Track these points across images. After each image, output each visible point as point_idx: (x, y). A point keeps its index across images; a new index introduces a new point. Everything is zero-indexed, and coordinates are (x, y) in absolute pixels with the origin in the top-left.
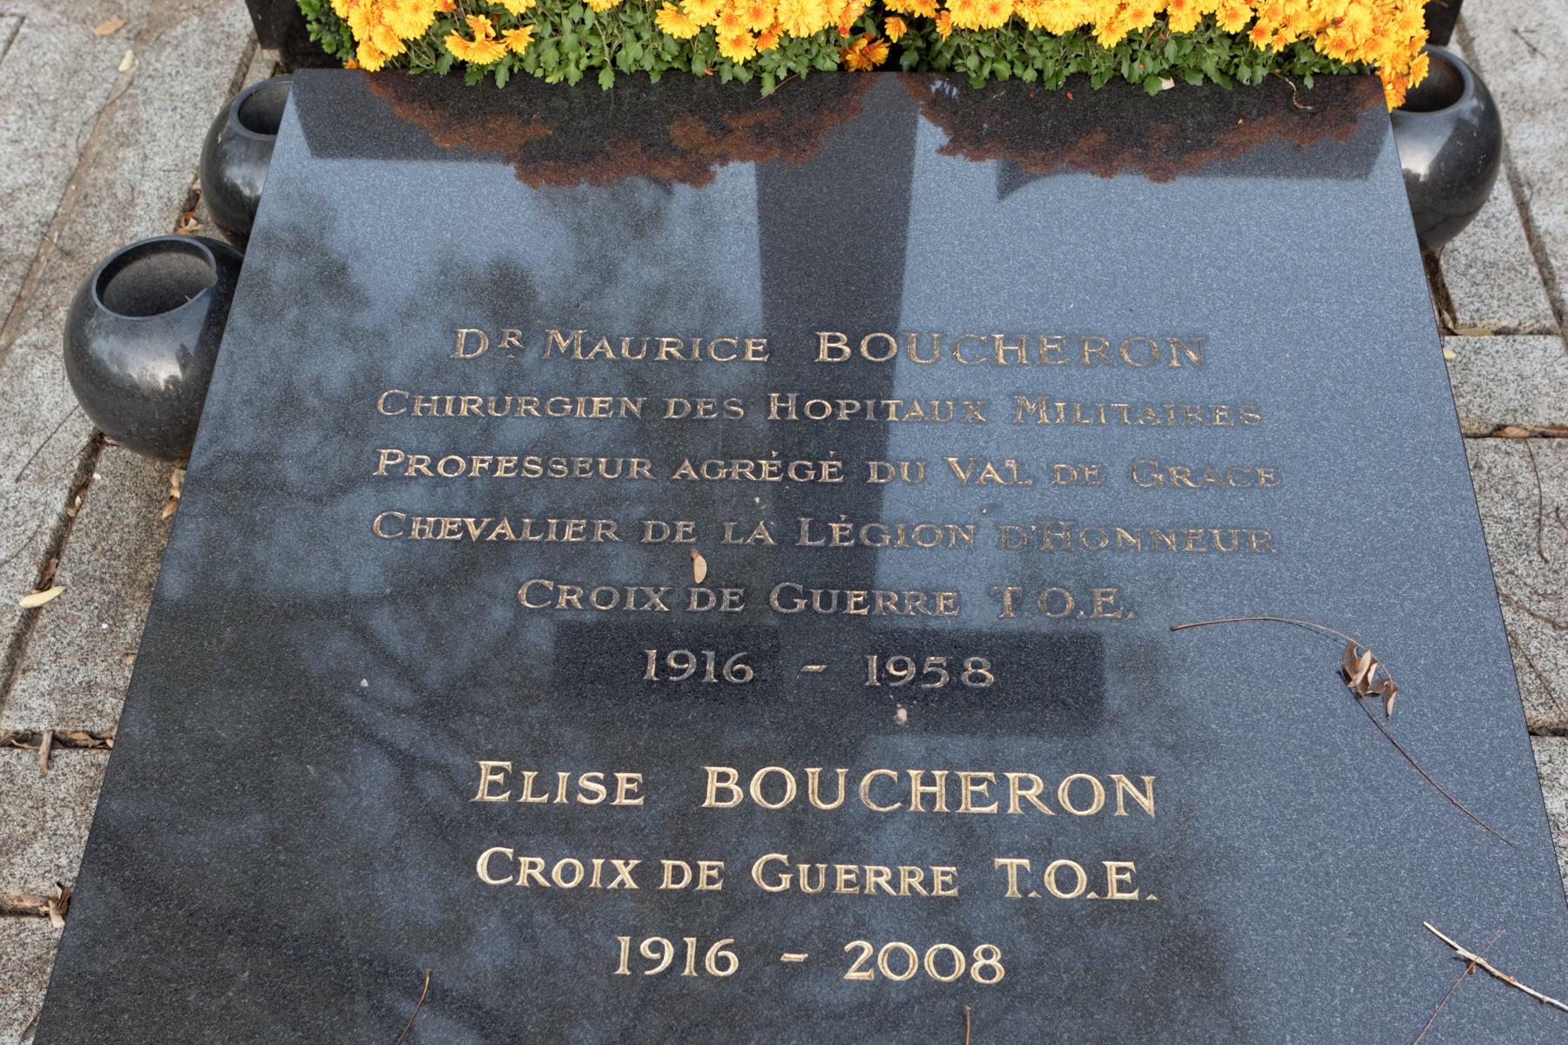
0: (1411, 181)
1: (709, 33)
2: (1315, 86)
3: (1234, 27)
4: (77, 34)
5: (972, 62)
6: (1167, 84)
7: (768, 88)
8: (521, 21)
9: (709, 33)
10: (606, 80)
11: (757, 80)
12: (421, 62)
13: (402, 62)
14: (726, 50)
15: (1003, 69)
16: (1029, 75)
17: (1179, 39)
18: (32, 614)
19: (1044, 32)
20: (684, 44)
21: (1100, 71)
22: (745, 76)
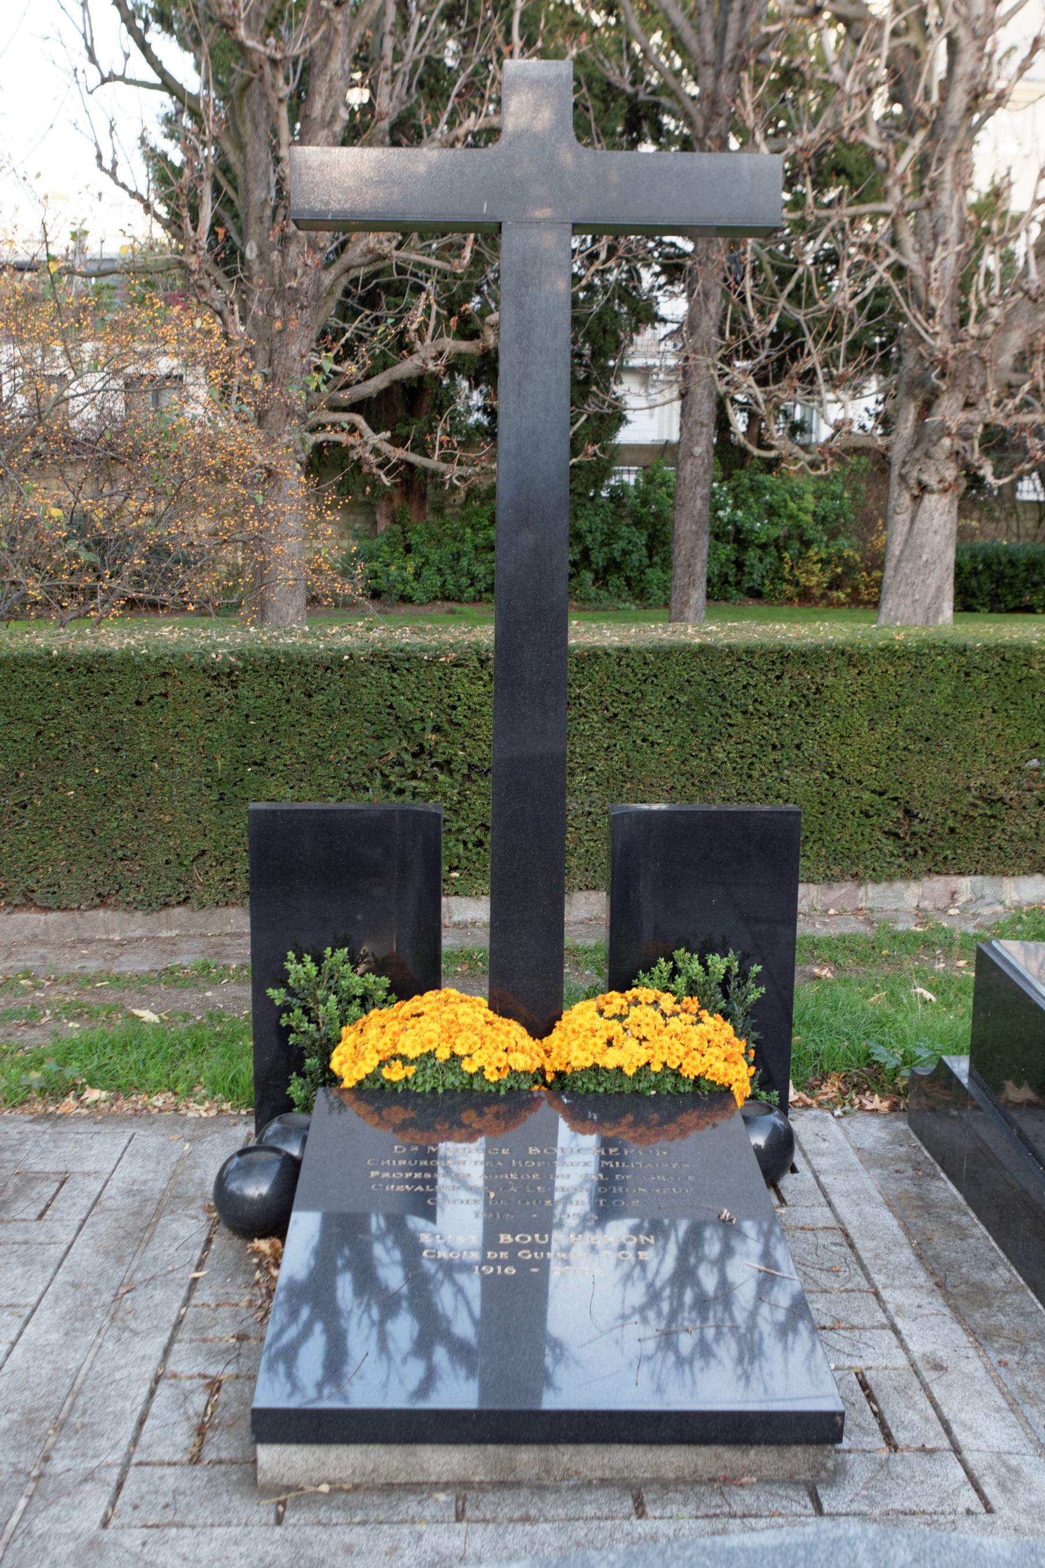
0: (757, 1150)
1: (482, 1069)
2: (550, 206)
3: (674, 1067)
4: (161, 1139)
5: (580, 1083)
6: (653, 1092)
7: (503, 1092)
8: (413, 1062)
9: (482, 1069)
10: (440, 1090)
11: (498, 1091)
12: (368, 1084)
13: (360, 1083)
14: (487, 1076)
15: (592, 1087)
16: (601, 1090)
17: (656, 1074)
18: (195, 1280)
19: (604, 1068)
20: (471, 1076)
21: (627, 1087)
22: (493, 1089)
